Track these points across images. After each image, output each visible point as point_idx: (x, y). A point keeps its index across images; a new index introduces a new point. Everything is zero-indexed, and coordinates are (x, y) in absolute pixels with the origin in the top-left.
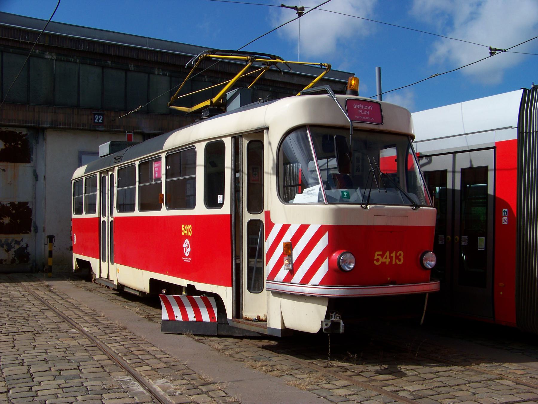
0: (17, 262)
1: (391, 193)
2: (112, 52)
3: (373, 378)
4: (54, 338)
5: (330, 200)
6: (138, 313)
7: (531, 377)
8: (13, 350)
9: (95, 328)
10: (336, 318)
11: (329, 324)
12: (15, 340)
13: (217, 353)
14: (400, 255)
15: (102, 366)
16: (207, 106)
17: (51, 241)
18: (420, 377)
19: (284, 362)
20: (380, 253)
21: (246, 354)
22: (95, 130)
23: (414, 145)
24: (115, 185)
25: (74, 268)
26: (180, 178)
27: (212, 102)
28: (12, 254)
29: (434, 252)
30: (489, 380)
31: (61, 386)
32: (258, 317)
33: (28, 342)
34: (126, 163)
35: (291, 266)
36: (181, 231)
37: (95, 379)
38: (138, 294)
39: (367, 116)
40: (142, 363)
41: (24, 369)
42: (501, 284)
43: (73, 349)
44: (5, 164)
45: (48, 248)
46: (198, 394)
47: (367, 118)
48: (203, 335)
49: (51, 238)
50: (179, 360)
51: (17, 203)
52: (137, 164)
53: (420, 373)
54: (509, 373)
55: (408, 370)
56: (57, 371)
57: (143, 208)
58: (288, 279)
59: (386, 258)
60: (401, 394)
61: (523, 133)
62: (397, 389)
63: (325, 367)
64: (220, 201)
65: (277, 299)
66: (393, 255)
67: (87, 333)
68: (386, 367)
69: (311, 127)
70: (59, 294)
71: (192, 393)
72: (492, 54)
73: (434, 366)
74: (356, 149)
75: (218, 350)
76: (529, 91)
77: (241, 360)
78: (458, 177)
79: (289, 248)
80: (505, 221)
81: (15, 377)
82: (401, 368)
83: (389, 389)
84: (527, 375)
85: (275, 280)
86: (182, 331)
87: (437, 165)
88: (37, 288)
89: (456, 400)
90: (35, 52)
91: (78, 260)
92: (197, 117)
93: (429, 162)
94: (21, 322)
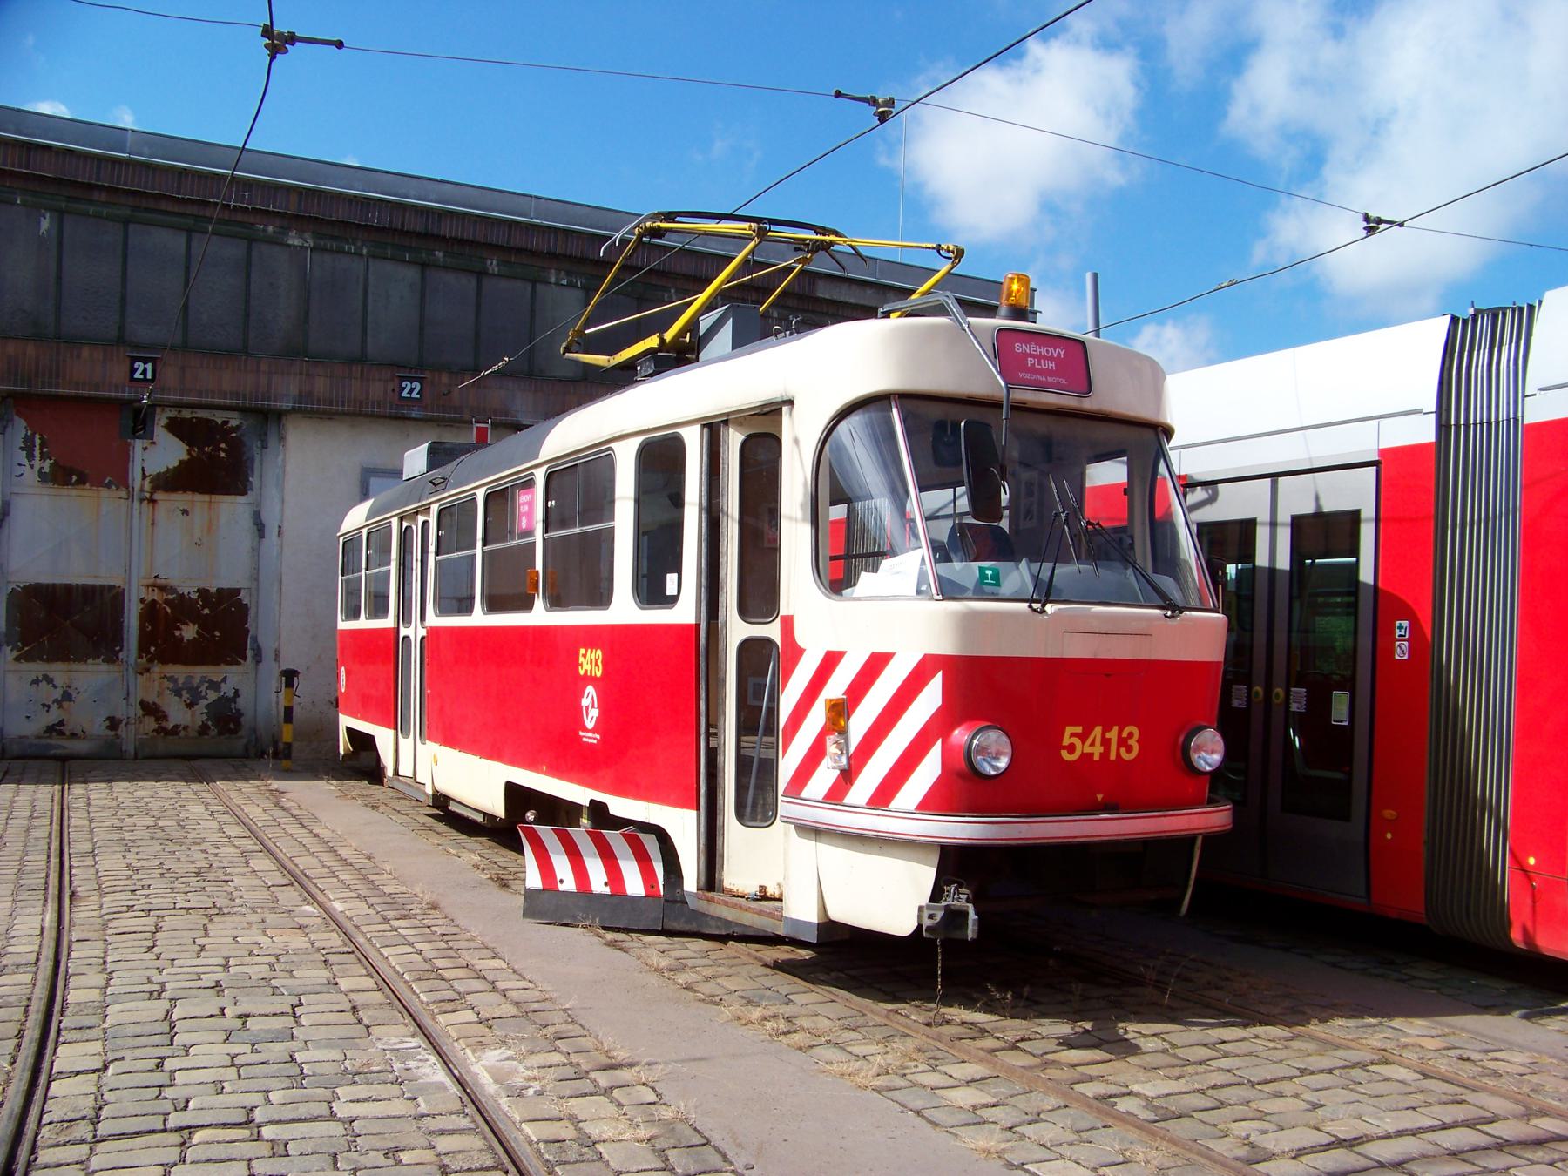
0: (214, 732)
1: (1109, 575)
2: (447, 230)
3: (1049, 1057)
4: (254, 930)
5: (949, 590)
6: (476, 866)
7: (1460, 1058)
8: (149, 956)
9: (363, 904)
10: (959, 899)
11: (939, 915)
12: (158, 929)
13: (653, 979)
14: (1131, 735)
15: (354, 1008)
16: (651, 351)
17: (289, 684)
18: (1175, 1056)
19: (823, 1007)
20: (1079, 729)
21: (730, 984)
22: (398, 417)
23: (1173, 456)
24: (432, 548)
25: (342, 751)
26: (577, 530)
27: (662, 341)
28: (199, 714)
29: (1223, 731)
30: (1355, 1065)
31: (237, 1061)
32: (763, 888)
33: (187, 937)
34: (454, 493)
35: (844, 760)
36: (577, 664)
37: (329, 1044)
38: (479, 818)
39: (1048, 372)
40: (457, 1001)
41: (161, 1006)
42: (1389, 814)
43: (295, 958)
44: (188, 496)
45: (283, 703)
46: (585, 1095)
47: (1050, 379)
48: (627, 930)
49: (290, 676)
50: (554, 995)
51: (213, 590)
52: (480, 495)
53: (1174, 1046)
54: (1406, 1046)
55: (1144, 1036)
56: (239, 1017)
57: (495, 603)
58: (836, 794)
59: (1093, 744)
60: (1123, 1105)
61: (1448, 426)
62: (1113, 1089)
63: (929, 1025)
64: (671, 589)
65: (809, 845)
66: (1113, 735)
67: (341, 918)
68: (1088, 1026)
69: (905, 398)
70: (296, 812)
71: (568, 1093)
72: (1370, 230)
73: (1212, 1026)
74: (1022, 456)
75: (657, 970)
76: (1465, 322)
77: (714, 1001)
78: (1284, 536)
79: (840, 714)
80: (1401, 651)
81: (131, 1030)
82: (1126, 1032)
83: (1090, 1089)
84: (1452, 1053)
85: (803, 795)
86: (574, 917)
87: (1230, 507)
88: (247, 796)
89: (1265, 1125)
90: (264, 231)
91: (351, 732)
92: (624, 377)
93: (1212, 499)
94: (187, 884)
